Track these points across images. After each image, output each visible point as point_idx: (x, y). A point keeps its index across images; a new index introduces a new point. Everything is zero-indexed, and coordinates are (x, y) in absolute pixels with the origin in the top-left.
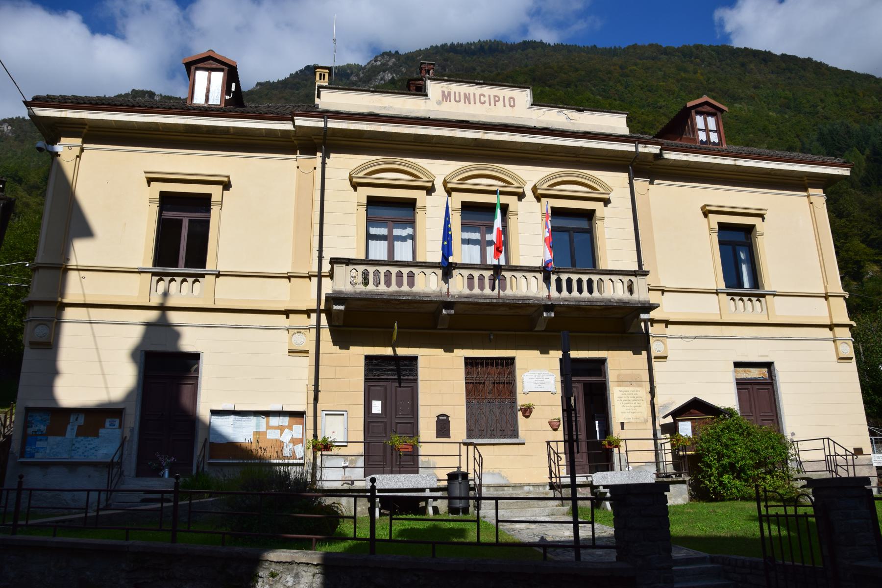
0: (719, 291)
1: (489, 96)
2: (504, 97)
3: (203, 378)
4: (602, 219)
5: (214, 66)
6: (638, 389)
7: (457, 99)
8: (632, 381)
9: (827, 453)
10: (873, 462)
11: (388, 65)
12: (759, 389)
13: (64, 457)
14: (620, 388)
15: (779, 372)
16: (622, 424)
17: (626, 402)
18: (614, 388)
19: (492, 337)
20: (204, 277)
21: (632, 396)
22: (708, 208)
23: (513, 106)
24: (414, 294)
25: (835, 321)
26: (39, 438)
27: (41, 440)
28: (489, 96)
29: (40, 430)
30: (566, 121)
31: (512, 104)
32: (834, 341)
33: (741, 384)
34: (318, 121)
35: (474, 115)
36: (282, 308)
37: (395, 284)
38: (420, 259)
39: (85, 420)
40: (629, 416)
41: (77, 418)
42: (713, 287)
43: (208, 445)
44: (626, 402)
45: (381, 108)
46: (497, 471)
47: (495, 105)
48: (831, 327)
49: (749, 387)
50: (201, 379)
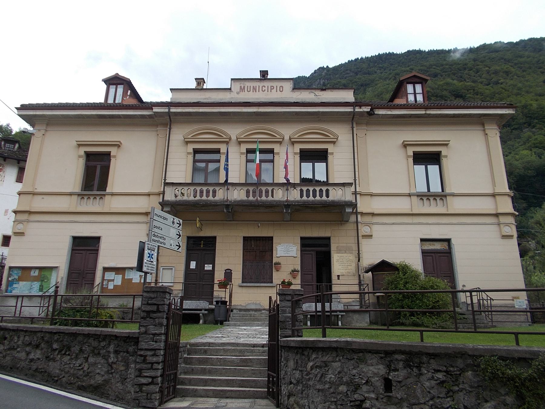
0: (411, 194)
1: (268, 86)
2: (277, 86)
4: (332, 154)
5: (119, 82)
6: (350, 255)
7: (249, 90)
8: (347, 250)
9: (479, 299)
10: (516, 305)
11: (322, 75)
13: (26, 293)
14: (339, 255)
15: (455, 245)
16: (338, 276)
17: (342, 263)
18: (334, 254)
19: (259, 225)
20: (105, 196)
21: (345, 259)
22: (406, 143)
23: (282, 91)
24: (275, 201)
25: (500, 211)
26: (15, 282)
27: (16, 284)
28: (268, 86)
30: (314, 97)
31: (281, 90)
33: (425, 254)
34: (166, 108)
35: (257, 99)
36: (144, 211)
37: (212, 196)
38: (331, 181)
39: (38, 273)
40: (342, 271)
43: (245, 284)
44: (342, 263)
45: (205, 99)
46: (258, 302)
47: (271, 91)
49: (433, 255)
50: (100, 250)
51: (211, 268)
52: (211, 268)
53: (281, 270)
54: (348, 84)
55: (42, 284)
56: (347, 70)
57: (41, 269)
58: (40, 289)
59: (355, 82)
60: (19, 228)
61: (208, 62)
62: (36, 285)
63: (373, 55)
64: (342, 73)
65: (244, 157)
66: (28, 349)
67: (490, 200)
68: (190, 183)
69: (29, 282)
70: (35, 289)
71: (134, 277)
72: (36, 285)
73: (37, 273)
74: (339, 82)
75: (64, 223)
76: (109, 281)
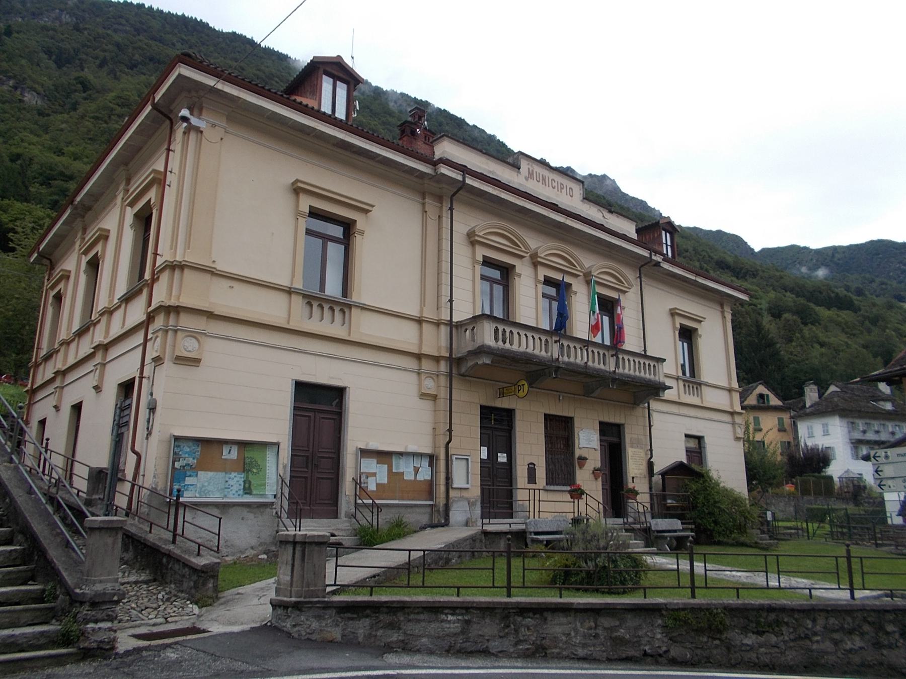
3: (350, 415)
5: (341, 75)
12: (323, 418)
22: (300, 185)
27: (190, 476)
29: (189, 464)
32: (419, 374)
34: (458, 174)
41: (230, 450)
42: (285, 282)
43: (552, 488)
48: (419, 357)
51: (505, 460)
52: (505, 460)
53: (585, 468)
54: (125, 45)
55: (247, 477)
56: (121, 17)
57: (243, 445)
58: (244, 488)
59: (140, 48)
60: (190, 349)
61: (353, 58)
62: (236, 479)
63: (173, 11)
64: (109, 18)
65: (303, 224)
66: (836, 636)
67: (413, 327)
68: (547, 331)
69: (220, 473)
70: (235, 488)
71: (407, 470)
72: (236, 480)
73: (236, 453)
74: (108, 35)
75: (255, 346)
76: (368, 475)
